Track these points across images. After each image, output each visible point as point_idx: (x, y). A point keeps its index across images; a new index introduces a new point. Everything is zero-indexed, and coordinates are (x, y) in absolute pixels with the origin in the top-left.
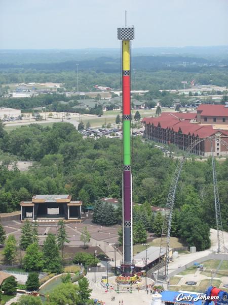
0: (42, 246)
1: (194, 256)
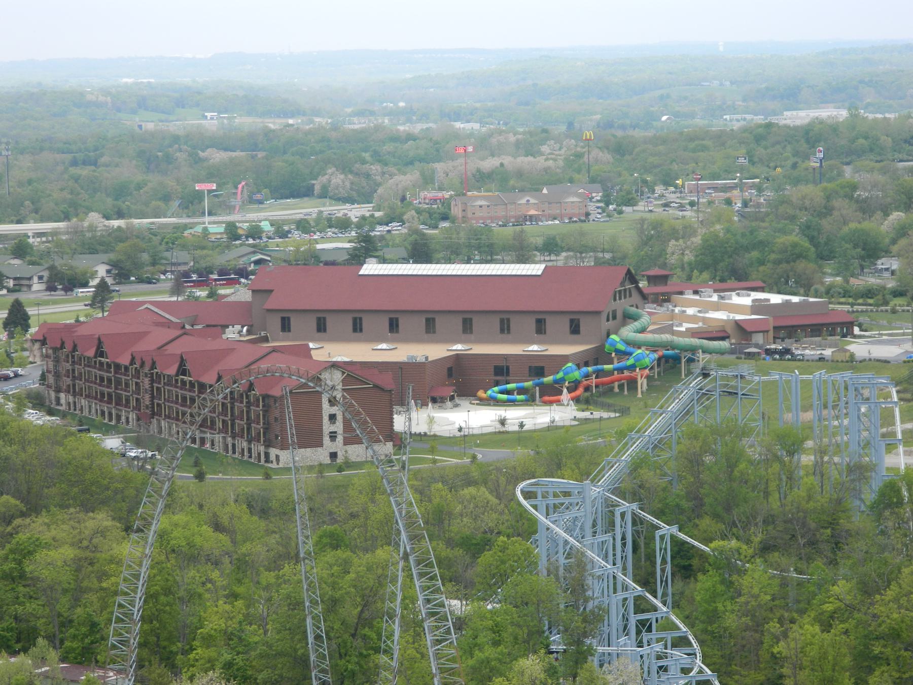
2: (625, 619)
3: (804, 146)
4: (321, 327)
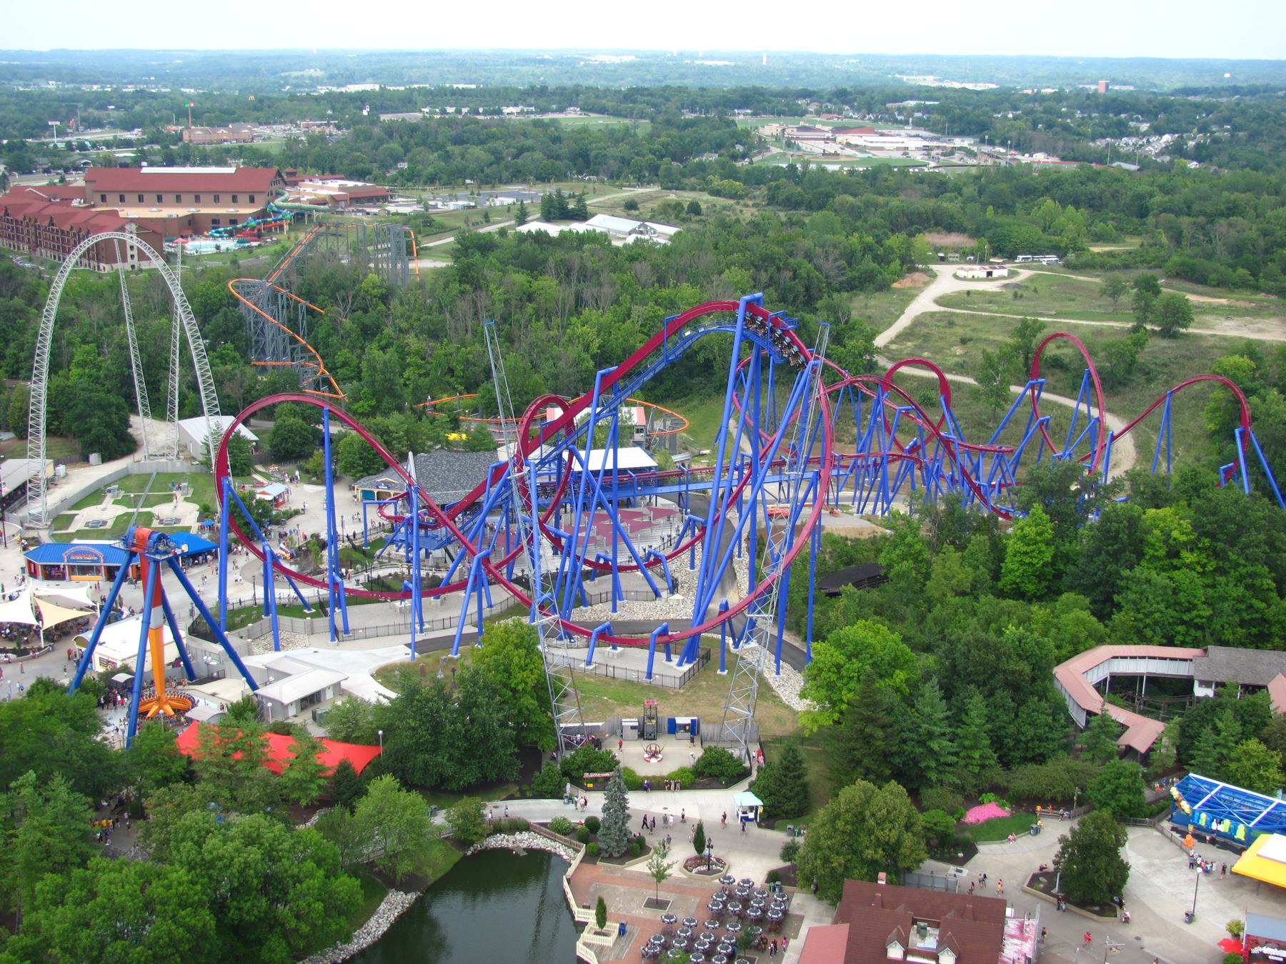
0: (361, 842)
1: (97, 471)
2: (285, 348)
3: (359, 103)
4: (122, 199)
